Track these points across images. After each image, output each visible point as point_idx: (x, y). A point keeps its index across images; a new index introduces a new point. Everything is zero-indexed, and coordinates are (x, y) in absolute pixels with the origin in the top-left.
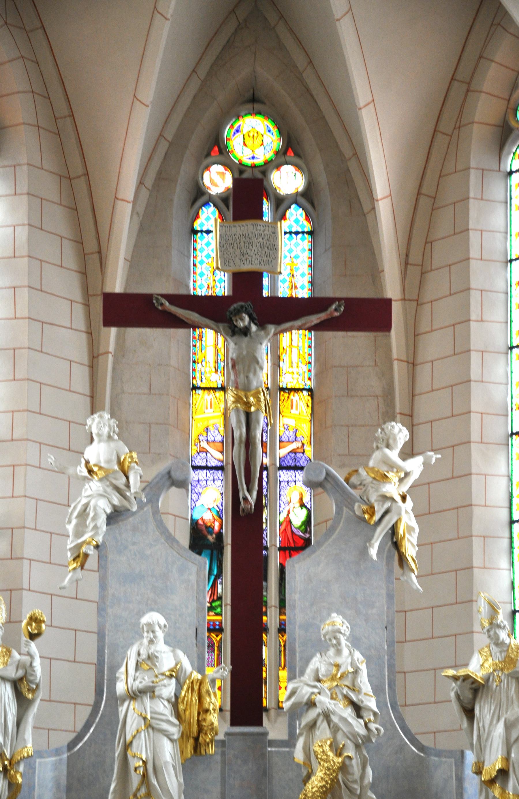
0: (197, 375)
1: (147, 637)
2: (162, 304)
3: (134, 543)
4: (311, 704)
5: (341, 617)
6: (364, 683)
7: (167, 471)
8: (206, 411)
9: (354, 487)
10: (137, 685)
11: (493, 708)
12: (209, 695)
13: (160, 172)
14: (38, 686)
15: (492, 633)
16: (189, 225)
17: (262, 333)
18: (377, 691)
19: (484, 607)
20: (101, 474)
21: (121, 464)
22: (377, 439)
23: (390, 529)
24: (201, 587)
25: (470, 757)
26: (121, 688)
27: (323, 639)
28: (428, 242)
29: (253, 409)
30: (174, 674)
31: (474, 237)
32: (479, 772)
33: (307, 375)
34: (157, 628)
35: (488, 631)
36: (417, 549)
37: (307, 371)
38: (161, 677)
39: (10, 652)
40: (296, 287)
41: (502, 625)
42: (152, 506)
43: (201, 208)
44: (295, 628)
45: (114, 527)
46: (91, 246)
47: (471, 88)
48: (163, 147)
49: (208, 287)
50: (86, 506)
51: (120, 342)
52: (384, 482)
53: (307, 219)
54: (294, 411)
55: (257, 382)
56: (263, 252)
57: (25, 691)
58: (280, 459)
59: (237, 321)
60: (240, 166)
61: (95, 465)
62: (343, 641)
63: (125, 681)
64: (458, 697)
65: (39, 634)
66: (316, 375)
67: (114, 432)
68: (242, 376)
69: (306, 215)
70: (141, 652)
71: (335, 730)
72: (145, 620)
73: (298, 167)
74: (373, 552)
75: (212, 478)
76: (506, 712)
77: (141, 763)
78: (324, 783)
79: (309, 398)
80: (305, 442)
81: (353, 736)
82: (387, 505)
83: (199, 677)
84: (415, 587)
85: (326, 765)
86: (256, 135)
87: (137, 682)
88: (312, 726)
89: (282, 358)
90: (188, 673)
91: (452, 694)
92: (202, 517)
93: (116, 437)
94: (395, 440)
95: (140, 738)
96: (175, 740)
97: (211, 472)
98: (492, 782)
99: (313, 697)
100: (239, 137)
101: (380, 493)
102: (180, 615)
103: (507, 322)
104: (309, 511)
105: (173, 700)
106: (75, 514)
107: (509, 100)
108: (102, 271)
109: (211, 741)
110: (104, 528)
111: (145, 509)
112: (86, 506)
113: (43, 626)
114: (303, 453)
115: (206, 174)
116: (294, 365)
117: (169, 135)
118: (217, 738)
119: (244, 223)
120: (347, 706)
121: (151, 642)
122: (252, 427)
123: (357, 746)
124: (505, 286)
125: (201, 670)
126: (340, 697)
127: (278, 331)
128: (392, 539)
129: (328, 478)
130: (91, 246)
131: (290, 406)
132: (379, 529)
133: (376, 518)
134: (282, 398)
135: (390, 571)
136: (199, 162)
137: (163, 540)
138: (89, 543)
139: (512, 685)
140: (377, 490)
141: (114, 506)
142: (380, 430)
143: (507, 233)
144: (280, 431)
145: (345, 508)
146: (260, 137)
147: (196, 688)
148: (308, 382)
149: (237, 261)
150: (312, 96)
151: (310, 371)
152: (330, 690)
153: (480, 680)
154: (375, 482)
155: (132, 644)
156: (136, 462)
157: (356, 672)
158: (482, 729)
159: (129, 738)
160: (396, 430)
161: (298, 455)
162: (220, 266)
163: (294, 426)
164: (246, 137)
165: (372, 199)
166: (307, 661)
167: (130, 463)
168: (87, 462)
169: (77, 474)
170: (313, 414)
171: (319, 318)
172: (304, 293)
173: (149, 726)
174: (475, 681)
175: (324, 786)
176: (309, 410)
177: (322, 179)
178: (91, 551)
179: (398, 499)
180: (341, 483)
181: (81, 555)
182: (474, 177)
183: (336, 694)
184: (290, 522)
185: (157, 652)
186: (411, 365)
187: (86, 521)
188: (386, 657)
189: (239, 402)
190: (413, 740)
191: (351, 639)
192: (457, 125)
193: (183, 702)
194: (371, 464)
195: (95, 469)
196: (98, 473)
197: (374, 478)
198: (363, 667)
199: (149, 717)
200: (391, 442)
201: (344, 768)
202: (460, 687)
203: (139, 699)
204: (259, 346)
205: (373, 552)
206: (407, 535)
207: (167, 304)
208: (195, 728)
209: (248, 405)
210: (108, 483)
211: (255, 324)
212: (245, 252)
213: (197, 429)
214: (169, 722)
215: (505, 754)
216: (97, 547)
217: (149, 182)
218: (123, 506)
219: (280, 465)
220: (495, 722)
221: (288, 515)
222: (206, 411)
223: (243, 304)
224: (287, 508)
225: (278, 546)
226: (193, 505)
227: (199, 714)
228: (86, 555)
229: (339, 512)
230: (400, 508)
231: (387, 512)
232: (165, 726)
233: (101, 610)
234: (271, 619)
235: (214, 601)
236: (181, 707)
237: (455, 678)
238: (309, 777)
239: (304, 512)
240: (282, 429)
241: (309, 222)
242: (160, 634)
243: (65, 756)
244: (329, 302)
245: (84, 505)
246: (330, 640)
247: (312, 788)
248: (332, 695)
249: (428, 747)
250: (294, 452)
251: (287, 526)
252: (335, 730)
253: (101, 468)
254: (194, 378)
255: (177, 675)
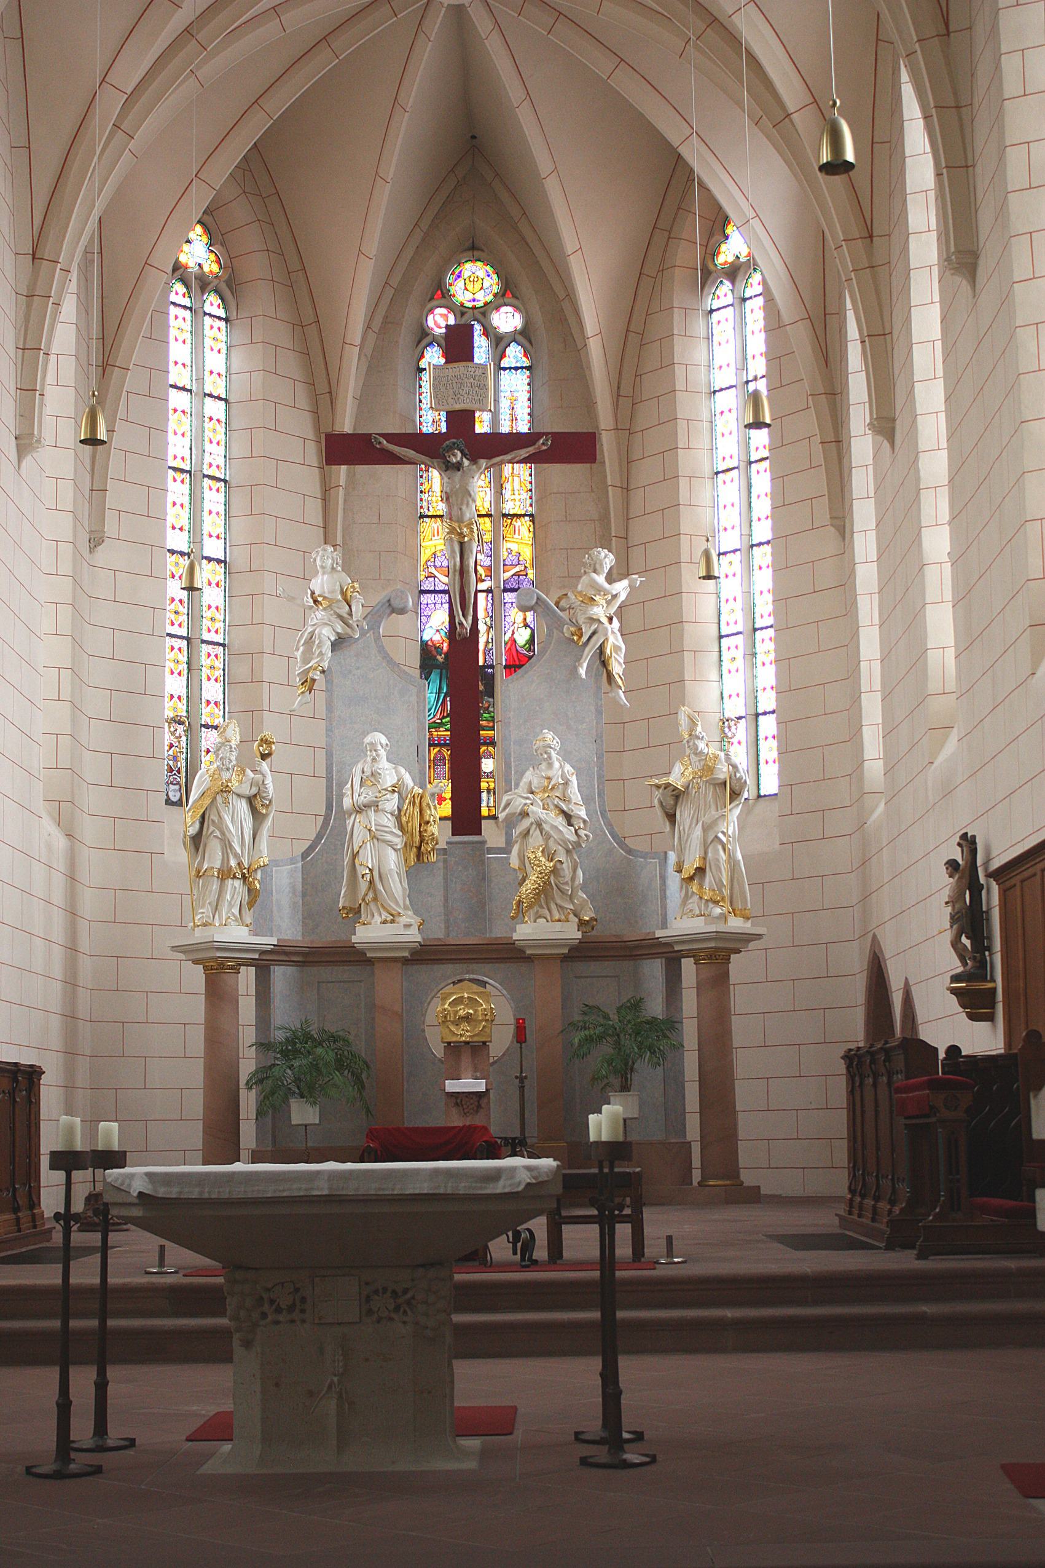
0: (425, 504)
1: (370, 756)
2: (380, 443)
3: (358, 668)
4: (525, 814)
5: (551, 733)
6: (575, 793)
7: (387, 599)
8: (433, 538)
9: (562, 610)
10: (362, 800)
11: (692, 812)
12: (430, 808)
13: (386, 317)
14: (270, 801)
15: (691, 744)
16: (414, 364)
17: (474, 467)
18: (587, 800)
19: (685, 720)
20: (325, 603)
21: (343, 593)
22: (584, 564)
23: (597, 649)
24: (421, 708)
25: (672, 857)
26: (347, 803)
27: (535, 754)
28: (638, 376)
29: (466, 539)
30: (396, 789)
31: (679, 371)
32: (680, 871)
33: (529, 501)
34: (379, 747)
35: (688, 742)
36: (624, 666)
37: (528, 497)
38: (384, 792)
39: (244, 771)
40: (516, 419)
41: (701, 736)
42: (373, 633)
43: (426, 347)
44: (510, 744)
45: (338, 653)
46: (322, 387)
47: (672, 236)
48: (390, 292)
49: (434, 421)
50: (312, 634)
51: (351, 478)
52: (592, 605)
53: (525, 355)
54: (516, 536)
55: (470, 514)
56: (474, 392)
57: (259, 807)
58: (504, 581)
59: (449, 457)
60: (461, 308)
61: (319, 596)
62: (553, 754)
63: (350, 796)
64: (661, 803)
65: (269, 755)
66: (537, 502)
67: (337, 564)
68: (455, 508)
69: (525, 351)
70: (365, 770)
71: (547, 837)
72: (368, 739)
73: (516, 308)
74: (582, 671)
75: (440, 601)
76: (704, 816)
77: (367, 871)
78: (537, 885)
79: (531, 523)
80: (527, 565)
81: (564, 842)
82: (593, 627)
83: (421, 791)
84: (622, 703)
85: (538, 869)
86: (476, 279)
87: (362, 798)
88: (526, 834)
89: (504, 486)
90: (410, 788)
91: (656, 802)
92: (431, 638)
93: (339, 568)
94: (601, 565)
95: (366, 847)
96: (399, 849)
97: (440, 595)
98: (691, 878)
99: (526, 808)
100: (460, 283)
101: (588, 616)
102: (402, 734)
103: (712, 449)
104: (533, 631)
105: (396, 813)
106: (302, 642)
107: (706, 246)
108: (332, 409)
109: (433, 849)
110: (330, 654)
111: (368, 635)
112: (312, 634)
113: (273, 747)
114: (526, 575)
115: (430, 318)
116: (516, 492)
117: (395, 282)
118: (437, 847)
119: (456, 365)
120: (558, 814)
121: (374, 760)
122: (465, 557)
123: (568, 851)
124: (709, 416)
125: (422, 786)
126: (552, 807)
127: (489, 465)
128: (600, 658)
129: (539, 602)
130: (322, 387)
131: (512, 532)
132: (587, 649)
133: (584, 639)
134: (505, 524)
135: (599, 688)
136: (423, 306)
137: (384, 664)
138: (315, 669)
139: (709, 790)
140: (584, 613)
141: (338, 633)
142: (587, 556)
143: (709, 366)
144: (504, 554)
145: (555, 630)
146: (480, 281)
147: (417, 801)
148: (530, 509)
149: (450, 400)
150: (527, 244)
151: (531, 498)
152: (542, 801)
153: (679, 787)
154: (582, 605)
155: (358, 762)
156: (358, 592)
157: (567, 783)
158: (682, 831)
159: (356, 849)
160: (603, 555)
161: (521, 577)
162: (433, 406)
163: (517, 550)
164: (467, 281)
165: (585, 338)
166: (522, 774)
167: (352, 592)
168: (313, 593)
169: (304, 604)
170: (534, 538)
171: (528, 452)
172: (523, 427)
173: (374, 837)
174: (676, 789)
175: (537, 888)
176: (531, 535)
177: (539, 319)
178: (317, 676)
179: (605, 620)
180: (552, 607)
181: (308, 680)
182: (677, 315)
183: (548, 805)
184: (514, 641)
185: (380, 769)
186: (625, 491)
187: (312, 648)
188: (596, 769)
189: (452, 533)
190: (622, 844)
191: (562, 753)
192: (661, 268)
193: (405, 815)
194: (579, 588)
195: (320, 599)
196: (322, 602)
197: (582, 601)
198: (574, 780)
199: (373, 829)
200: (598, 566)
201: (555, 871)
202: (663, 794)
203: (364, 813)
204: (471, 480)
205: (582, 671)
206: (613, 654)
207: (385, 442)
208: (417, 839)
209: (461, 535)
210: (332, 612)
211: (468, 459)
212: (457, 392)
213: (425, 555)
214: (392, 833)
215: (702, 855)
216: (323, 672)
217: (377, 324)
218: (347, 634)
219: (505, 587)
220: (693, 825)
221: (513, 634)
222: (433, 538)
223: (455, 440)
224: (512, 629)
225: (504, 664)
226: (423, 627)
227: (420, 825)
228: (314, 680)
229: (550, 634)
230: (607, 629)
231: (594, 633)
232: (389, 837)
233: (329, 730)
234: (498, 733)
235: (444, 717)
236: (404, 819)
237: (658, 787)
238: (524, 880)
239: (528, 631)
240: (506, 554)
241: (528, 358)
242: (382, 753)
243: (300, 864)
244: (539, 435)
245: (309, 633)
246: (542, 755)
247: (526, 891)
248: (543, 805)
249: (635, 850)
250: (517, 574)
251: (512, 645)
252: (547, 837)
253: (325, 598)
254: (421, 507)
255: (399, 789)
